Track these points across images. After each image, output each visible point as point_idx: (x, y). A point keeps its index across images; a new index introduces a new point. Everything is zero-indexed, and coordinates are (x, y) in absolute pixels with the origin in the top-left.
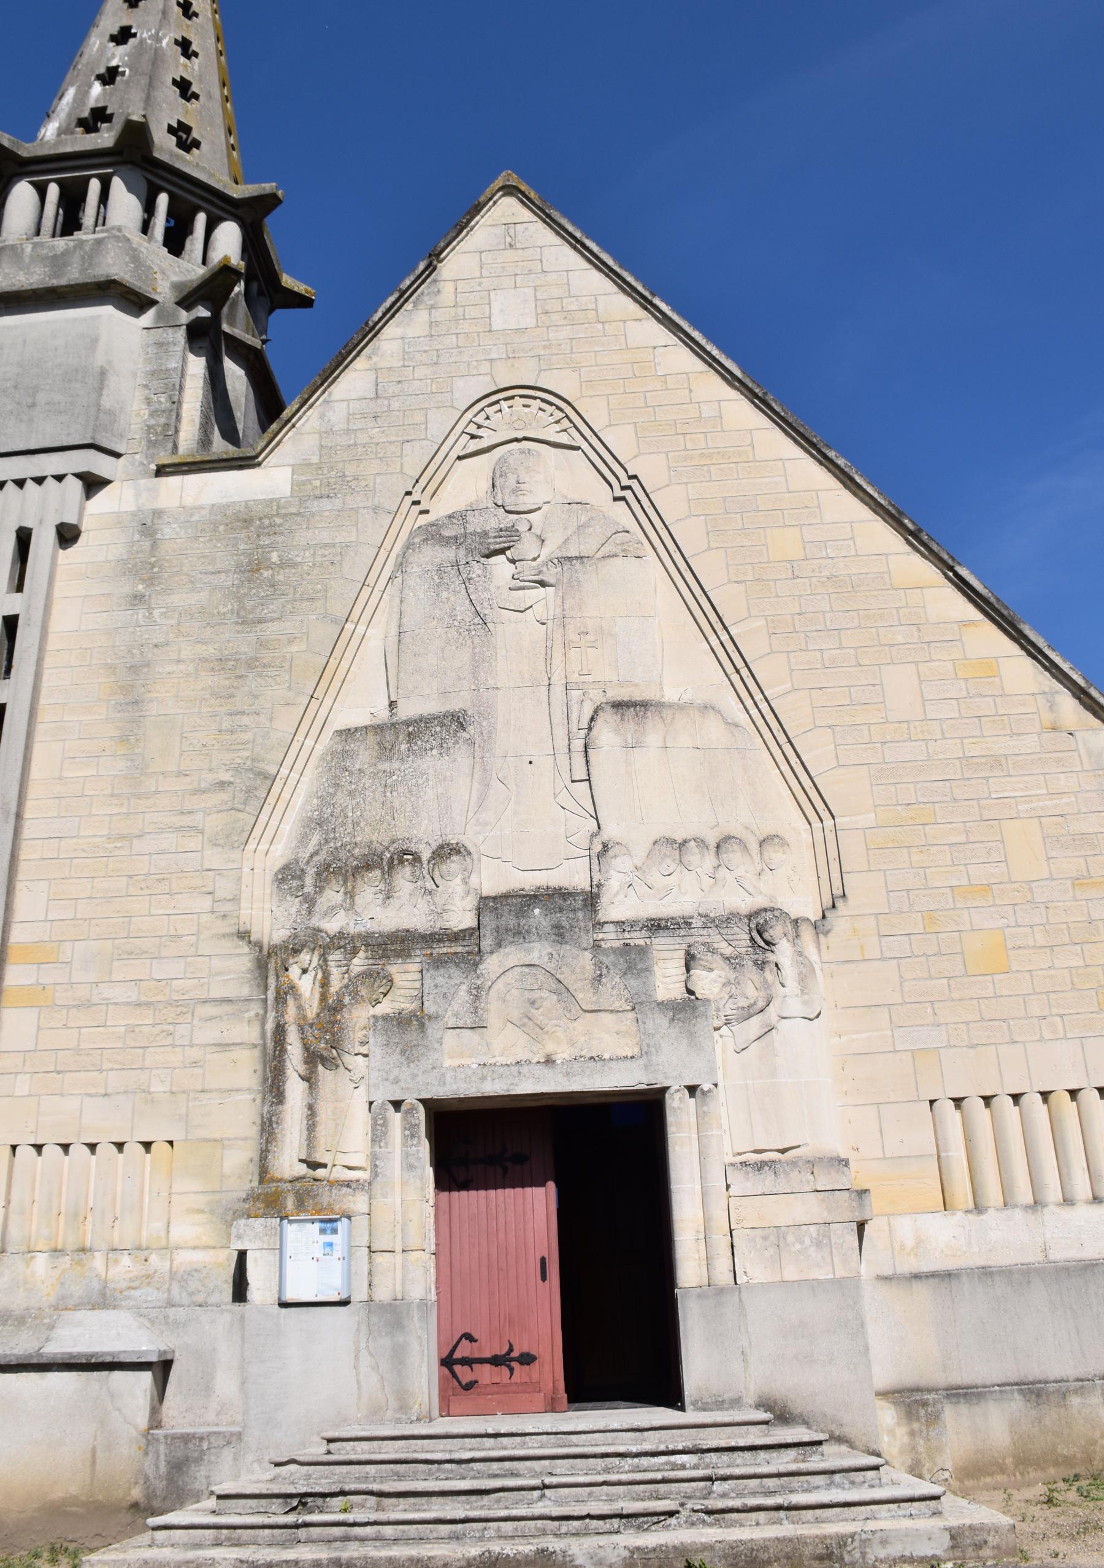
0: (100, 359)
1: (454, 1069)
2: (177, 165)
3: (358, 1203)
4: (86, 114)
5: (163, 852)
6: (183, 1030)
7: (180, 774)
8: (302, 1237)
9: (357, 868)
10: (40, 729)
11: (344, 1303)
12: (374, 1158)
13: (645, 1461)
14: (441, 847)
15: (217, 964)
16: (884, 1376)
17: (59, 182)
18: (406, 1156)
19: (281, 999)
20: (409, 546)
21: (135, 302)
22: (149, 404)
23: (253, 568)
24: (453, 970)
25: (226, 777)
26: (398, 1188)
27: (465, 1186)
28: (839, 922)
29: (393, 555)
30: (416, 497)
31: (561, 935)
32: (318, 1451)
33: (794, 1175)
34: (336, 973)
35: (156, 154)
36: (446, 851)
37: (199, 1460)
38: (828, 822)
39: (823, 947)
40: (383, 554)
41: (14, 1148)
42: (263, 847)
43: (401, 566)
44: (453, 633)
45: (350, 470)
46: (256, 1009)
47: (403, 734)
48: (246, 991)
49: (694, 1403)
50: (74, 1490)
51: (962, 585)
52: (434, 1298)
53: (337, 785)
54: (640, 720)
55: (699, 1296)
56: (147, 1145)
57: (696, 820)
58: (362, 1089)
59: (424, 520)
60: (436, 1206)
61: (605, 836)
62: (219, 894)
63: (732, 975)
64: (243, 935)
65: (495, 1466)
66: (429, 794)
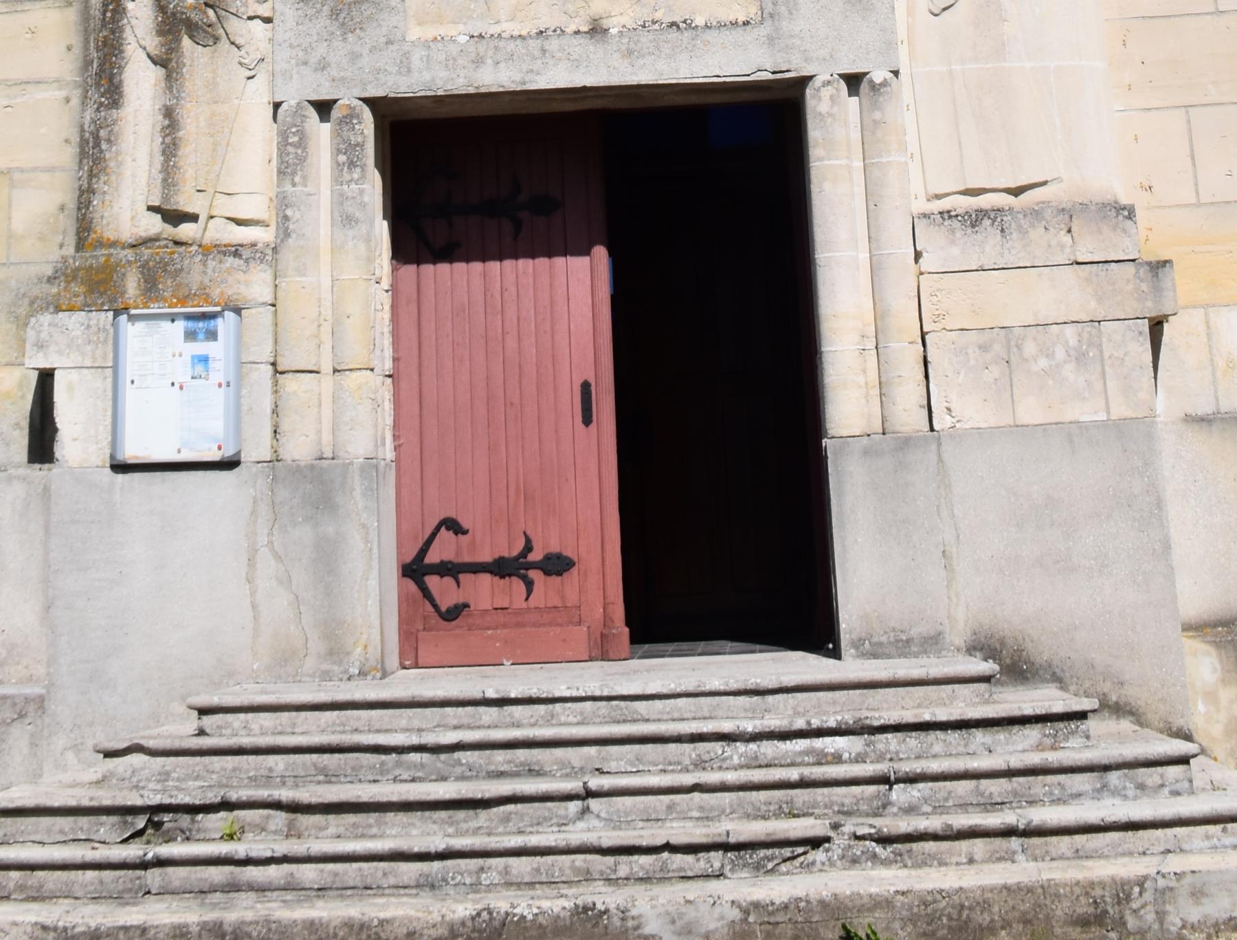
1: (427, 45)
3: (254, 285)
11: (229, 464)
12: (282, 204)
13: (769, 749)
16: (1197, 595)
18: (340, 199)
26: (325, 257)
32: (181, 730)
33: (1037, 234)
49: (857, 644)
52: (389, 454)
55: (866, 452)
58: (262, 79)
60: (394, 290)
65: (500, 756)
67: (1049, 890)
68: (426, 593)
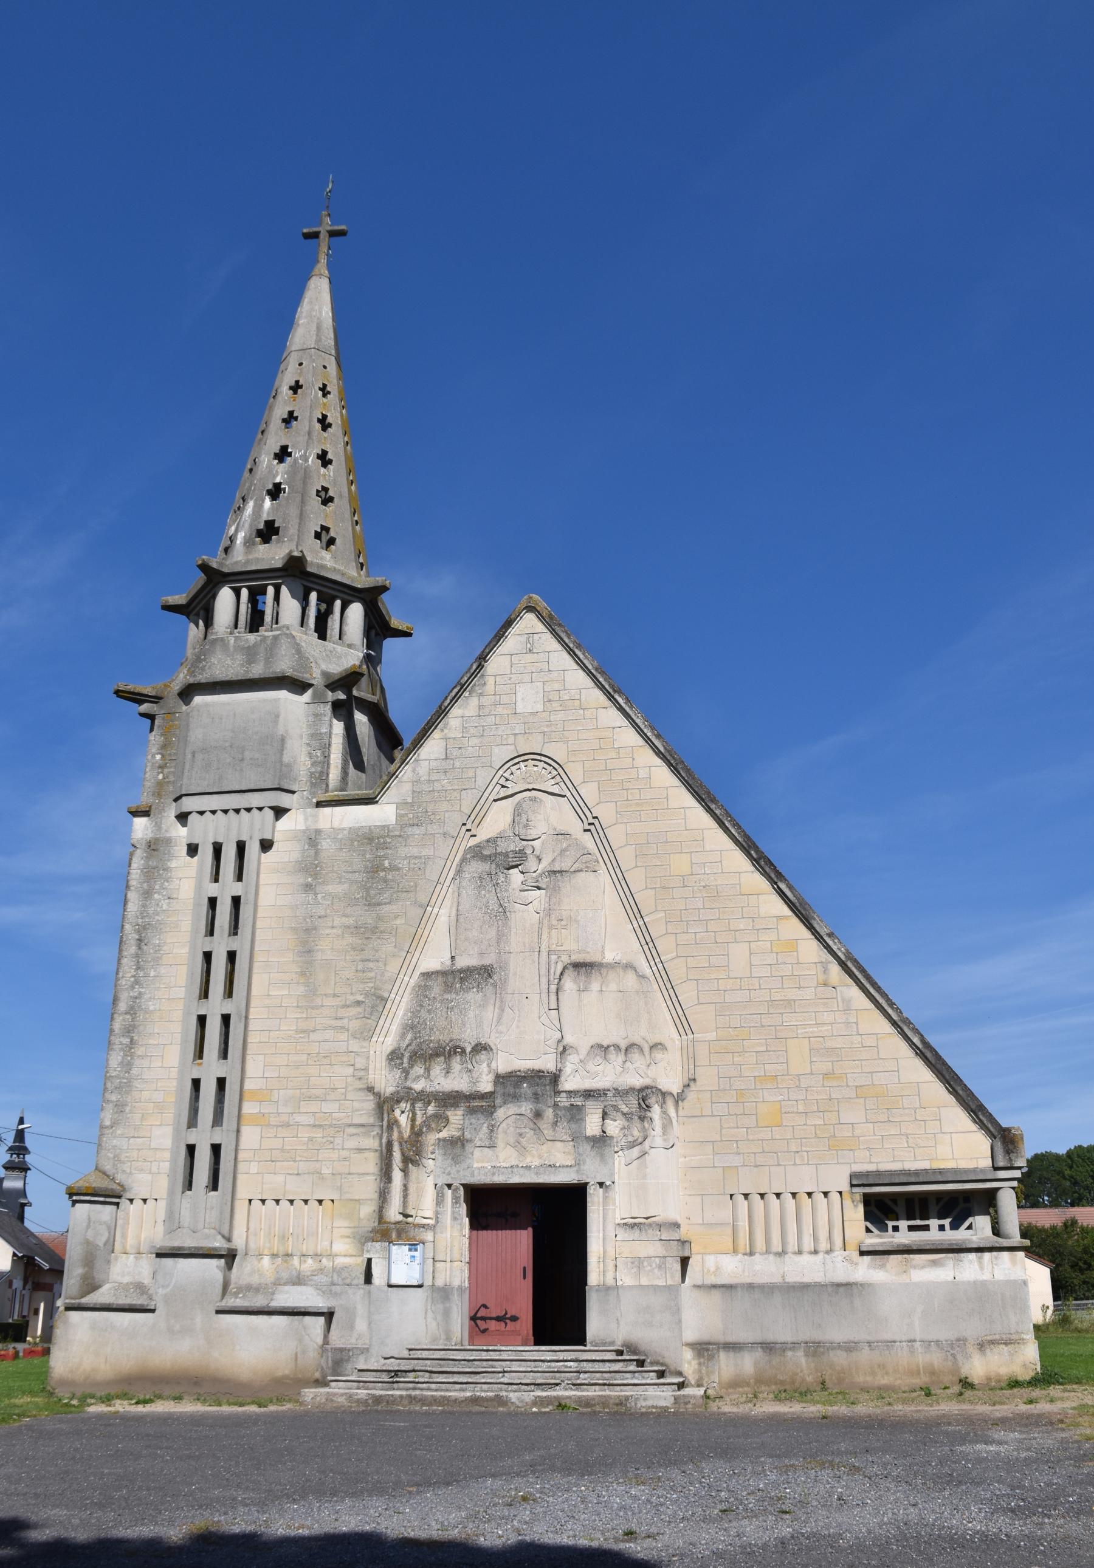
0: (281, 730)
1: (479, 1169)
2: (322, 574)
3: (429, 1236)
4: (261, 526)
5: (326, 1041)
6: (338, 1141)
7: (335, 995)
8: (400, 1252)
9: (431, 1055)
10: (256, 965)
11: (420, 1286)
12: (437, 1213)
13: (553, 1364)
14: (477, 1045)
15: (356, 1105)
16: (691, 1334)
17: (248, 587)
18: (453, 1213)
19: (390, 1127)
20: (463, 860)
21: (298, 686)
22: (311, 757)
23: (374, 869)
24: (480, 1116)
25: (361, 998)
26: (449, 1229)
27: (485, 1228)
28: (691, 1096)
29: (455, 864)
30: (468, 827)
31: (537, 1099)
32: (406, 1354)
33: (650, 1231)
34: (419, 1113)
35: (309, 569)
36: (480, 1048)
37: (348, 1360)
38: (690, 1036)
39: (680, 1108)
40: (449, 863)
41: (250, 1201)
42: (381, 1039)
43: (459, 872)
44: (487, 917)
45: (431, 807)
46: (377, 1130)
47: (458, 978)
48: (371, 1120)
49: (591, 1343)
50: (287, 1372)
51: (781, 893)
52: (467, 1284)
53: (421, 1006)
54: (588, 975)
55: (597, 1290)
56: (320, 1202)
57: (616, 1035)
58: (431, 1177)
59: (473, 842)
60: (470, 1238)
61: (565, 1042)
62: (358, 1066)
63: (626, 1124)
64: (370, 1089)
65: (485, 1363)
66: (471, 1014)
67: (609, 1397)
68: (477, 1325)
